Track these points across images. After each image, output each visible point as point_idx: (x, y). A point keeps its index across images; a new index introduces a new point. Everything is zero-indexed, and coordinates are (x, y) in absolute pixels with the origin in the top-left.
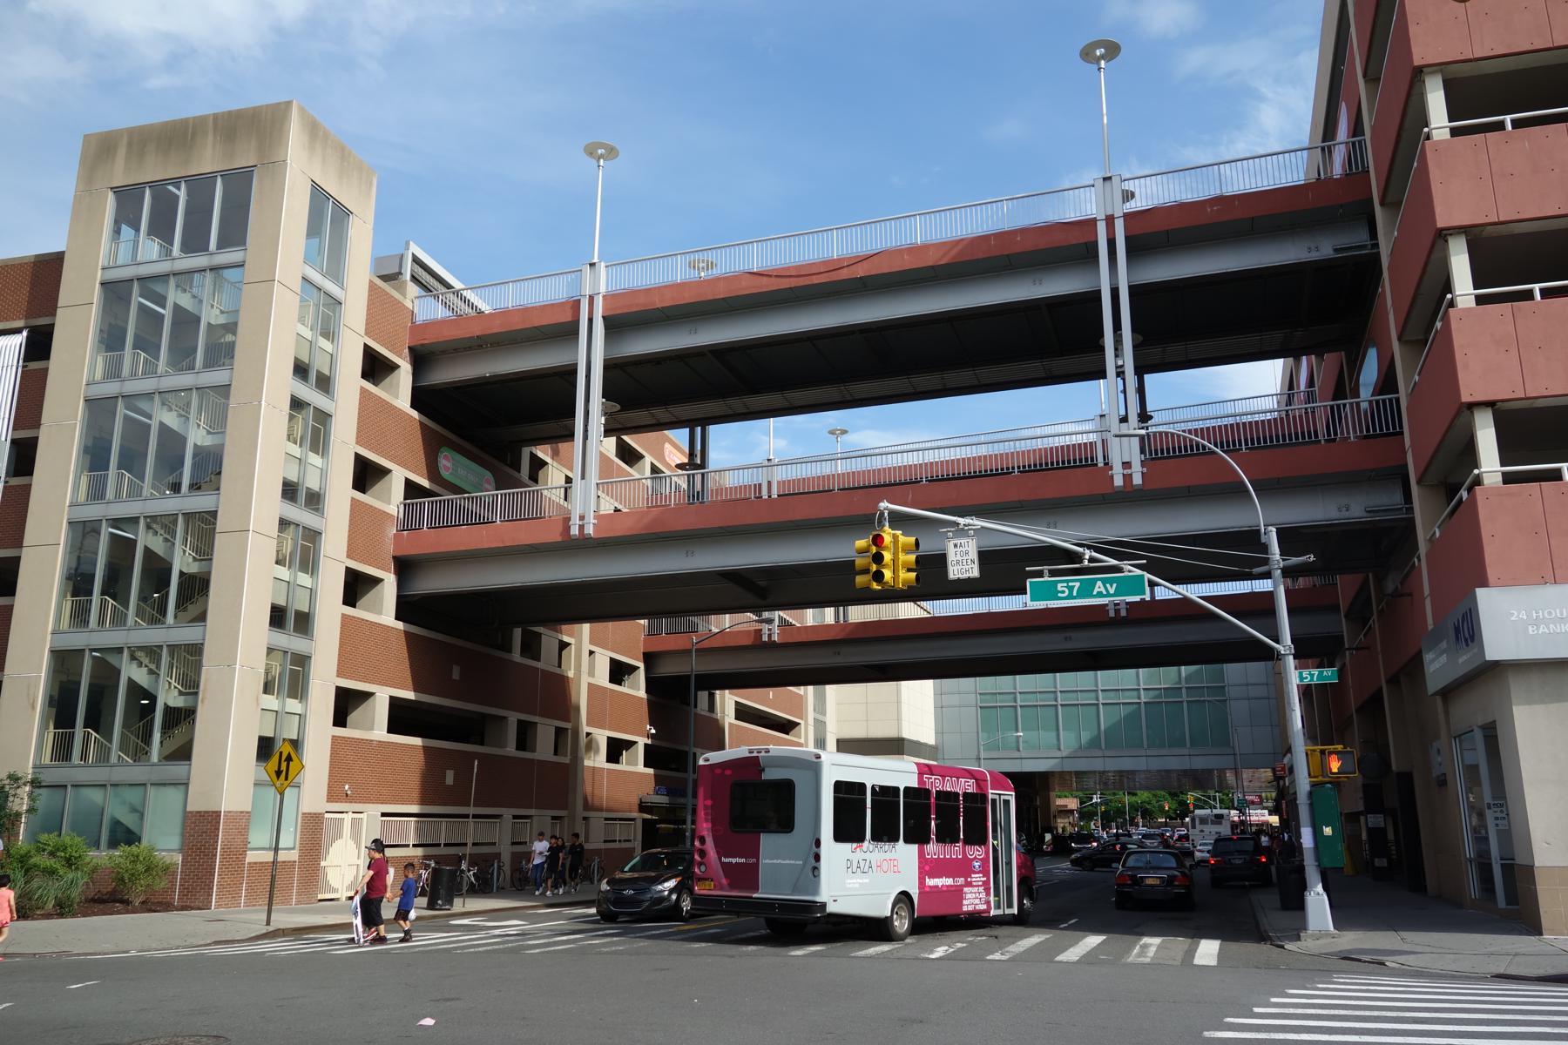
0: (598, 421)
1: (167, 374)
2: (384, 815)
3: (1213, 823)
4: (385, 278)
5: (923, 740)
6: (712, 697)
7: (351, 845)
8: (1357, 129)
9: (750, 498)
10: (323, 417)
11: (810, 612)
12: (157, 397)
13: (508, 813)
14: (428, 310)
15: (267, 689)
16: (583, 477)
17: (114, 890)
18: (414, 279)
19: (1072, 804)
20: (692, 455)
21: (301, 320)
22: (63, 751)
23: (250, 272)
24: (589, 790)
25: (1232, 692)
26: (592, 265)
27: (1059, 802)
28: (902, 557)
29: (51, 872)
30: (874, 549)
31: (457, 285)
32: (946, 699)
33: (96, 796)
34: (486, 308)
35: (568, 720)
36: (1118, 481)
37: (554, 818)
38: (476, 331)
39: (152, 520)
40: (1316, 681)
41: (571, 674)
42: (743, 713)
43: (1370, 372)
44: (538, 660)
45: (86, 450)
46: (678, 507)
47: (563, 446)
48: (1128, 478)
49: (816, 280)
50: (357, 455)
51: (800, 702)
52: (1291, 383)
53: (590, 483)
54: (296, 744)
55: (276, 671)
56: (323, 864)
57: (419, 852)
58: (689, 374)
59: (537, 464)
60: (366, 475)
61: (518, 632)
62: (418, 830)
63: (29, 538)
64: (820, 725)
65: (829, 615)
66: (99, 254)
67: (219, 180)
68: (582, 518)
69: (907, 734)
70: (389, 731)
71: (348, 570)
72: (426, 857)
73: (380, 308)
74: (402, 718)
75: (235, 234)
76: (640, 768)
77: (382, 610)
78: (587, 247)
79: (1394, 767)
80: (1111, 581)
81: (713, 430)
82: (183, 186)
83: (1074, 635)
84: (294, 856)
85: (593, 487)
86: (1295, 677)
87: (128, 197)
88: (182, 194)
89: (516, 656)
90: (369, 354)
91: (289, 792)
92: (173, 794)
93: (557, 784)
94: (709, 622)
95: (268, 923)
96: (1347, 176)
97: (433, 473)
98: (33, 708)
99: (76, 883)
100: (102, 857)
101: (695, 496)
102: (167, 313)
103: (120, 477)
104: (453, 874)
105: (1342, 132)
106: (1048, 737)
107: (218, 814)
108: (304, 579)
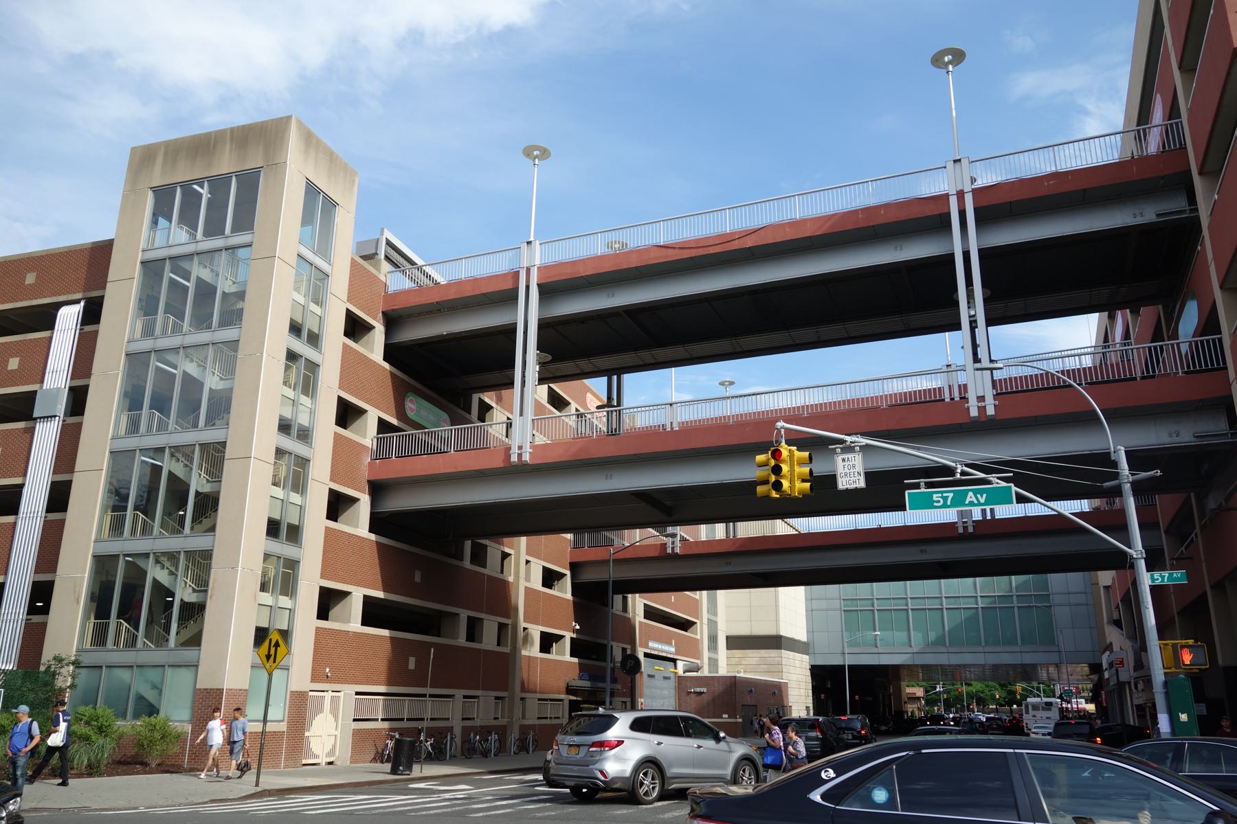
0: (533, 370)
1: (190, 333)
2: (357, 693)
3: (1044, 709)
4: (365, 258)
5: (797, 638)
6: (625, 600)
7: (331, 718)
8: (1173, 111)
9: (656, 433)
10: (313, 367)
11: (703, 528)
12: (181, 351)
13: (459, 693)
14: (397, 282)
15: (263, 588)
16: (521, 415)
17: (137, 754)
18: (387, 258)
19: (920, 692)
20: (609, 398)
21: (297, 289)
22: (100, 638)
23: (256, 251)
24: (525, 675)
25: (1055, 599)
26: (529, 243)
27: (909, 690)
28: (797, 469)
29: (87, 738)
30: (773, 462)
31: (420, 262)
32: (816, 604)
33: (125, 675)
34: (442, 280)
35: (508, 617)
36: (974, 412)
37: (497, 698)
38: (435, 298)
39: (176, 450)
40: (1166, 582)
41: (511, 579)
42: (650, 613)
43: (1190, 319)
44: (485, 567)
45: (126, 394)
46: (599, 438)
47: (505, 393)
48: (982, 410)
49: (712, 250)
50: (339, 398)
51: (695, 607)
52: (1106, 338)
53: (526, 420)
54: (285, 634)
55: (272, 574)
56: (307, 734)
57: (386, 725)
58: (611, 329)
59: (485, 409)
60: (347, 414)
61: (468, 544)
62: (386, 708)
63: (79, 465)
64: (713, 624)
65: (720, 531)
66: (140, 240)
67: (234, 179)
68: (520, 448)
69: (784, 632)
70: (363, 624)
71: (331, 491)
72: (392, 730)
73: (360, 279)
74: (373, 613)
75: (245, 221)
76: (567, 657)
77: (358, 523)
78: (525, 220)
79: (1220, 662)
80: (981, 492)
81: (627, 378)
82: (206, 184)
83: (929, 548)
84: (283, 727)
85: (530, 422)
86: (1146, 580)
87: (163, 196)
88: (205, 192)
89: (467, 564)
90: (350, 316)
91: (277, 674)
92: (186, 674)
93: (499, 670)
94: (623, 539)
95: (257, 785)
96: (1164, 152)
97: (401, 413)
98: (78, 602)
99: (105, 747)
100: (127, 726)
101: (612, 433)
102: (191, 285)
103: (151, 417)
104: (412, 744)
105: (1158, 115)
106: (901, 636)
107: (221, 691)
108: (295, 498)
